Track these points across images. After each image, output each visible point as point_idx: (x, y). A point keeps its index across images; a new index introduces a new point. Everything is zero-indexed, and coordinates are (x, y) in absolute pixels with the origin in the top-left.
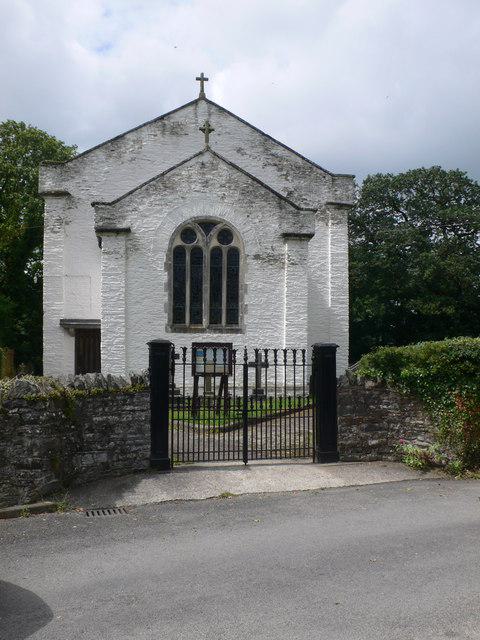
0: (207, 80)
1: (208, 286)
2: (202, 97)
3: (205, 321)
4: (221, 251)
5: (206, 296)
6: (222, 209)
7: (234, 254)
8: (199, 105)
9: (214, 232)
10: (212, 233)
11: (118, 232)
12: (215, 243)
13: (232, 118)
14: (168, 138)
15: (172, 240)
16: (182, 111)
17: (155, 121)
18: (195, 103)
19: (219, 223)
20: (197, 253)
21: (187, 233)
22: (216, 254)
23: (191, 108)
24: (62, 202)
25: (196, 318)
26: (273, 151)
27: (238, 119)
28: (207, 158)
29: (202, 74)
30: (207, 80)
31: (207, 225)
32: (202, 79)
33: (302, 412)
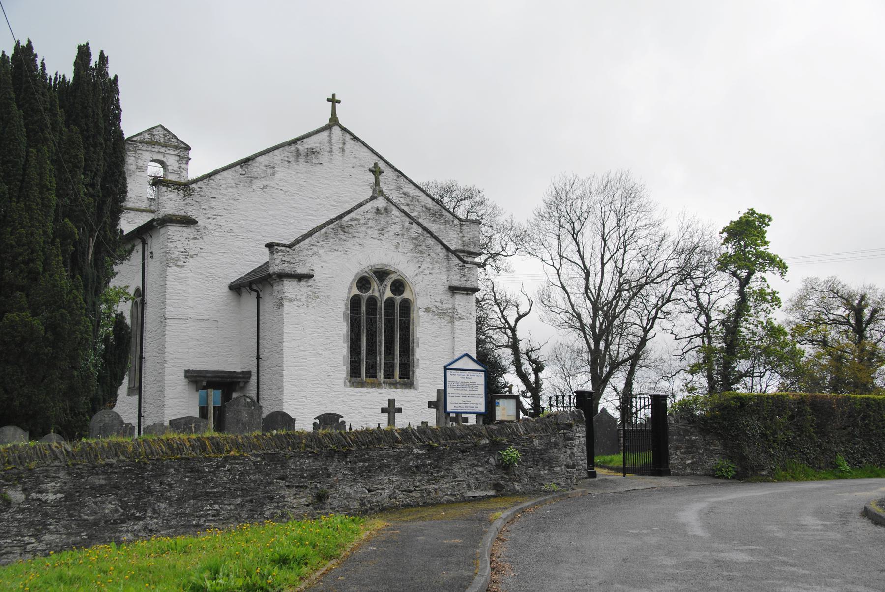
0: (339, 102)
3: (381, 375)
4: (394, 302)
6: (401, 263)
7: (406, 306)
8: (333, 131)
9: (388, 282)
10: (385, 283)
11: (300, 277)
12: (388, 294)
13: (366, 149)
14: (302, 166)
16: (370, 153)
18: (328, 128)
20: (372, 301)
21: (363, 283)
22: (390, 303)
23: (325, 134)
24: (187, 232)
25: (372, 373)
26: (405, 190)
28: (380, 203)
29: (334, 95)
30: (339, 102)
31: (382, 274)
32: (333, 101)
33: (646, 404)
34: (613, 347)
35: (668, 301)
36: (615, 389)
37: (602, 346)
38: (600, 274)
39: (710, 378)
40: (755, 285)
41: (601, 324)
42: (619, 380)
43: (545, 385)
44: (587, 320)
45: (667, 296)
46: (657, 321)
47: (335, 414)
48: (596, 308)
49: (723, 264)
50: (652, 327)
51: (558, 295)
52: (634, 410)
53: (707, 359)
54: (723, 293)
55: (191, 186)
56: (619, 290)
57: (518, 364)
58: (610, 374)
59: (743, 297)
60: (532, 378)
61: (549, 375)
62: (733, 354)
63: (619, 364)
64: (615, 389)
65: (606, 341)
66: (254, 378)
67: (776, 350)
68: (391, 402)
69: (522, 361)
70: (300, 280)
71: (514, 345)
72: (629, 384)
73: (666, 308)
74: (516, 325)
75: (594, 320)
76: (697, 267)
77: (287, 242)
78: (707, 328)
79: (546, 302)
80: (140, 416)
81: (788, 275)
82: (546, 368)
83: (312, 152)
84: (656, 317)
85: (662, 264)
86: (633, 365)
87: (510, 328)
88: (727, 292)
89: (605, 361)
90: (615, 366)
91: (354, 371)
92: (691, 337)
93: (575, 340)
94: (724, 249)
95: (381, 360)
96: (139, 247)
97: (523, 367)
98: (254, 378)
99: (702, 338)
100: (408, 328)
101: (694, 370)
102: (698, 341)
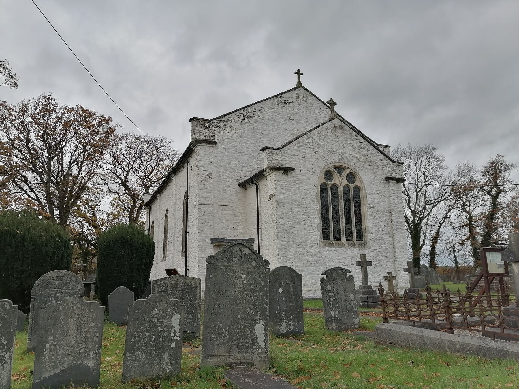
0: (302, 74)
1: (196, 244)
2: (299, 85)
3: (344, 238)
5: (342, 220)
7: (357, 190)
9: (345, 173)
12: (345, 183)
15: (361, 180)
17: (272, 97)
18: (297, 88)
19: (348, 168)
20: (335, 188)
22: (347, 187)
27: (317, 98)
28: (337, 122)
29: (298, 70)
30: (302, 74)
31: (340, 169)
32: (298, 74)
35: (453, 208)
47: (342, 269)
55: (213, 122)
66: (256, 242)
68: (364, 257)
77: (276, 147)
80: (186, 269)
83: (286, 102)
91: (326, 236)
95: (343, 227)
96: (186, 164)
98: (256, 242)
100: (359, 206)
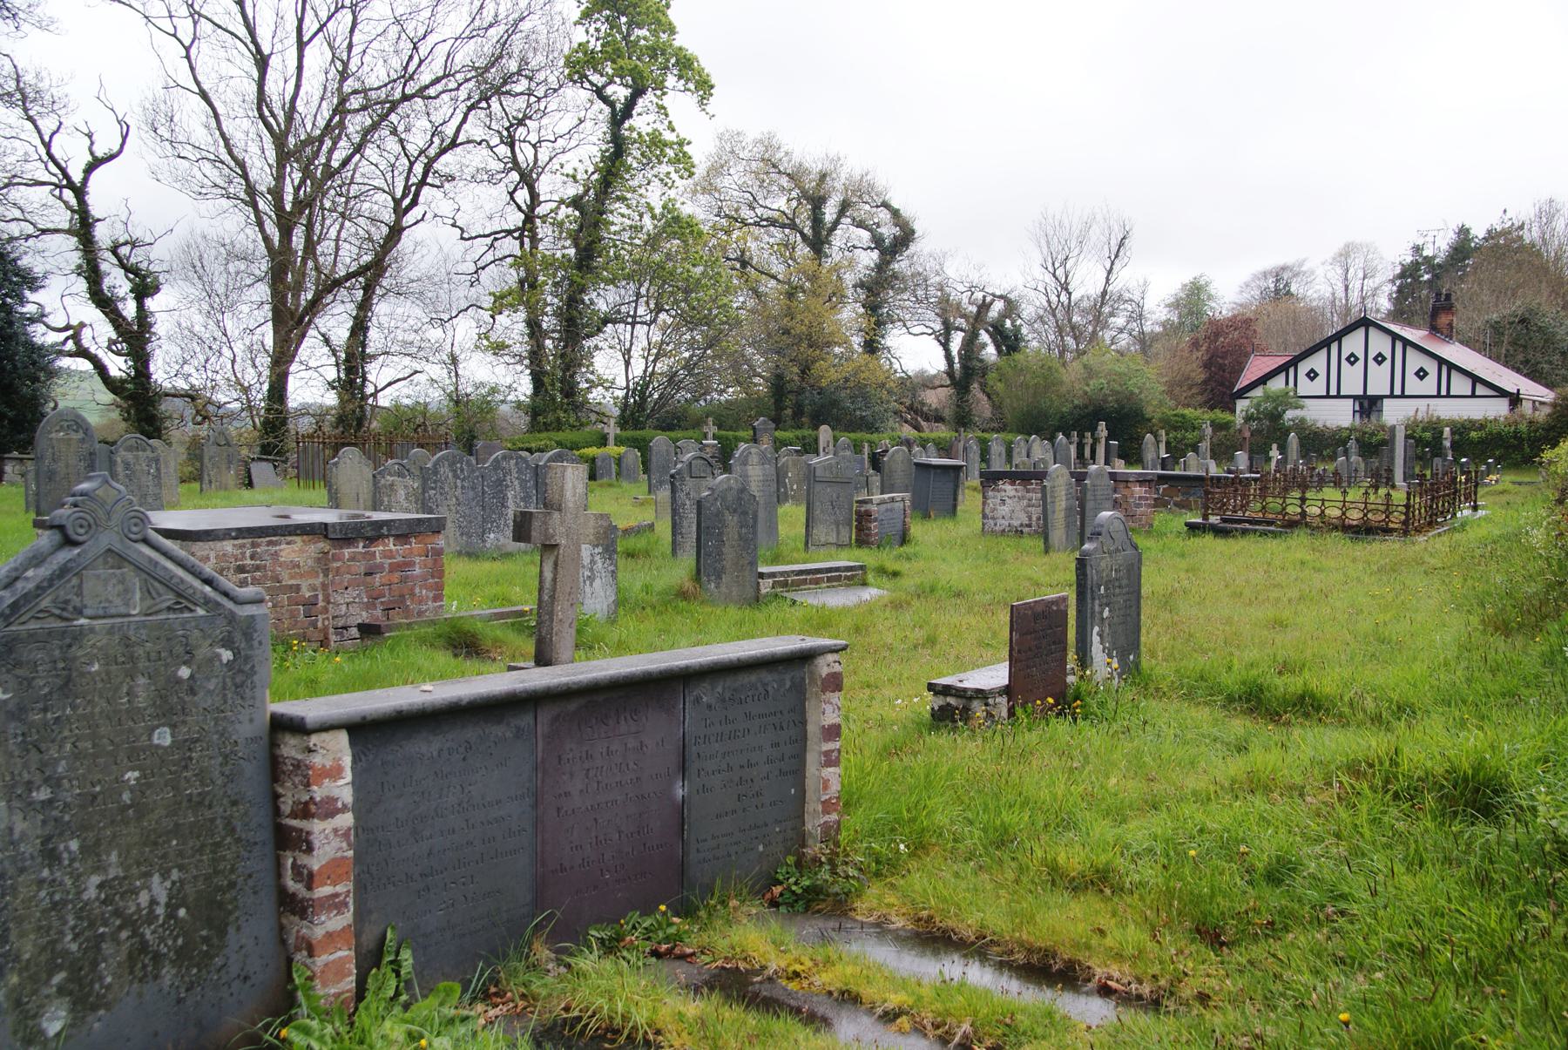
34: (326, 247)
35: (454, 144)
36: (327, 341)
37: (298, 240)
38: (293, 81)
39: (533, 325)
40: (642, 122)
41: (297, 190)
42: (336, 321)
43: (162, 326)
44: (262, 175)
45: (449, 130)
46: (426, 190)
48: (283, 156)
49: (580, 66)
50: (414, 203)
51: (192, 114)
52: (370, 389)
53: (529, 283)
54: (570, 136)
56: (341, 110)
57: (92, 273)
58: (315, 306)
59: (618, 147)
60: (129, 309)
61: (173, 304)
62: (590, 269)
63: (338, 283)
64: (327, 341)
65: (309, 227)
67: (675, 270)
69: (104, 267)
70: (79, 271)
71: (84, 227)
72: (360, 328)
73: (446, 163)
74: (85, 181)
75: (280, 178)
76: (519, 73)
78: (529, 218)
79: (162, 131)
81: (714, 104)
82: (165, 289)
84: (423, 182)
85: (442, 50)
86: (368, 289)
87: (71, 185)
88: (573, 143)
89: (304, 275)
90: (331, 285)
92: (495, 236)
93: (233, 225)
94: (579, 35)
97: (107, 283)
99: (521, 238)
101: (500, 303)
102: (510, 246)
